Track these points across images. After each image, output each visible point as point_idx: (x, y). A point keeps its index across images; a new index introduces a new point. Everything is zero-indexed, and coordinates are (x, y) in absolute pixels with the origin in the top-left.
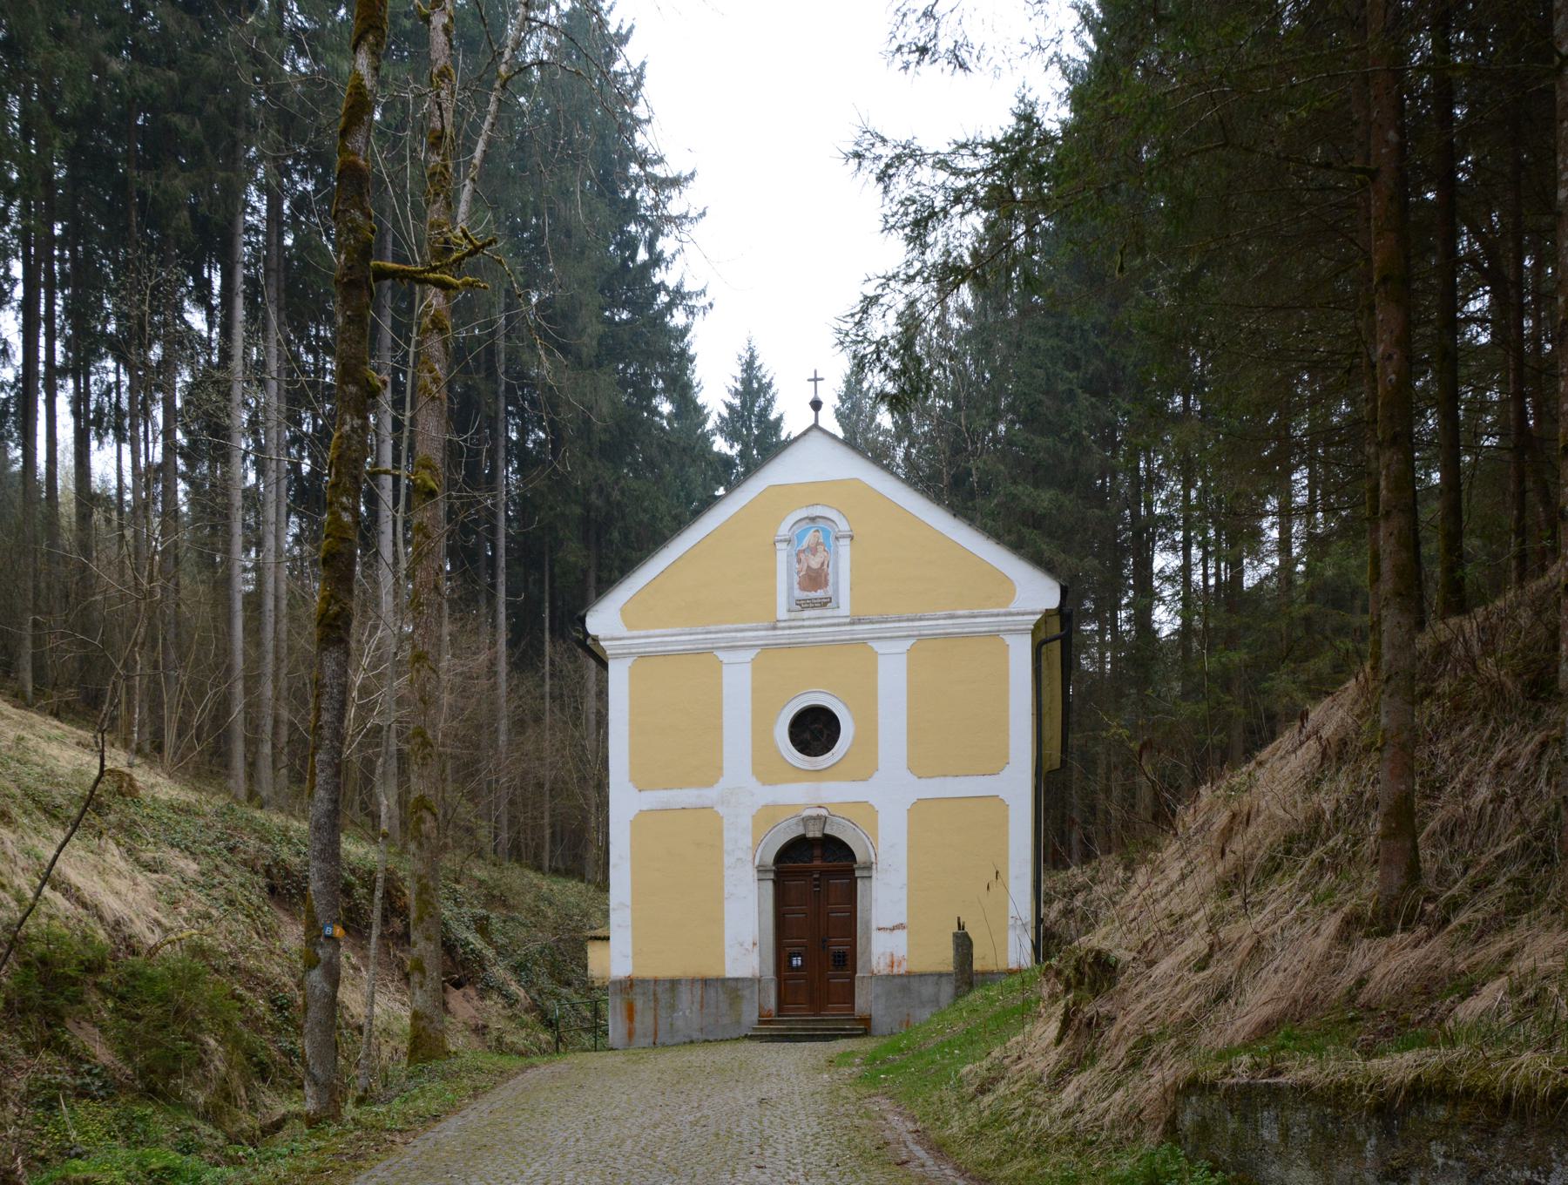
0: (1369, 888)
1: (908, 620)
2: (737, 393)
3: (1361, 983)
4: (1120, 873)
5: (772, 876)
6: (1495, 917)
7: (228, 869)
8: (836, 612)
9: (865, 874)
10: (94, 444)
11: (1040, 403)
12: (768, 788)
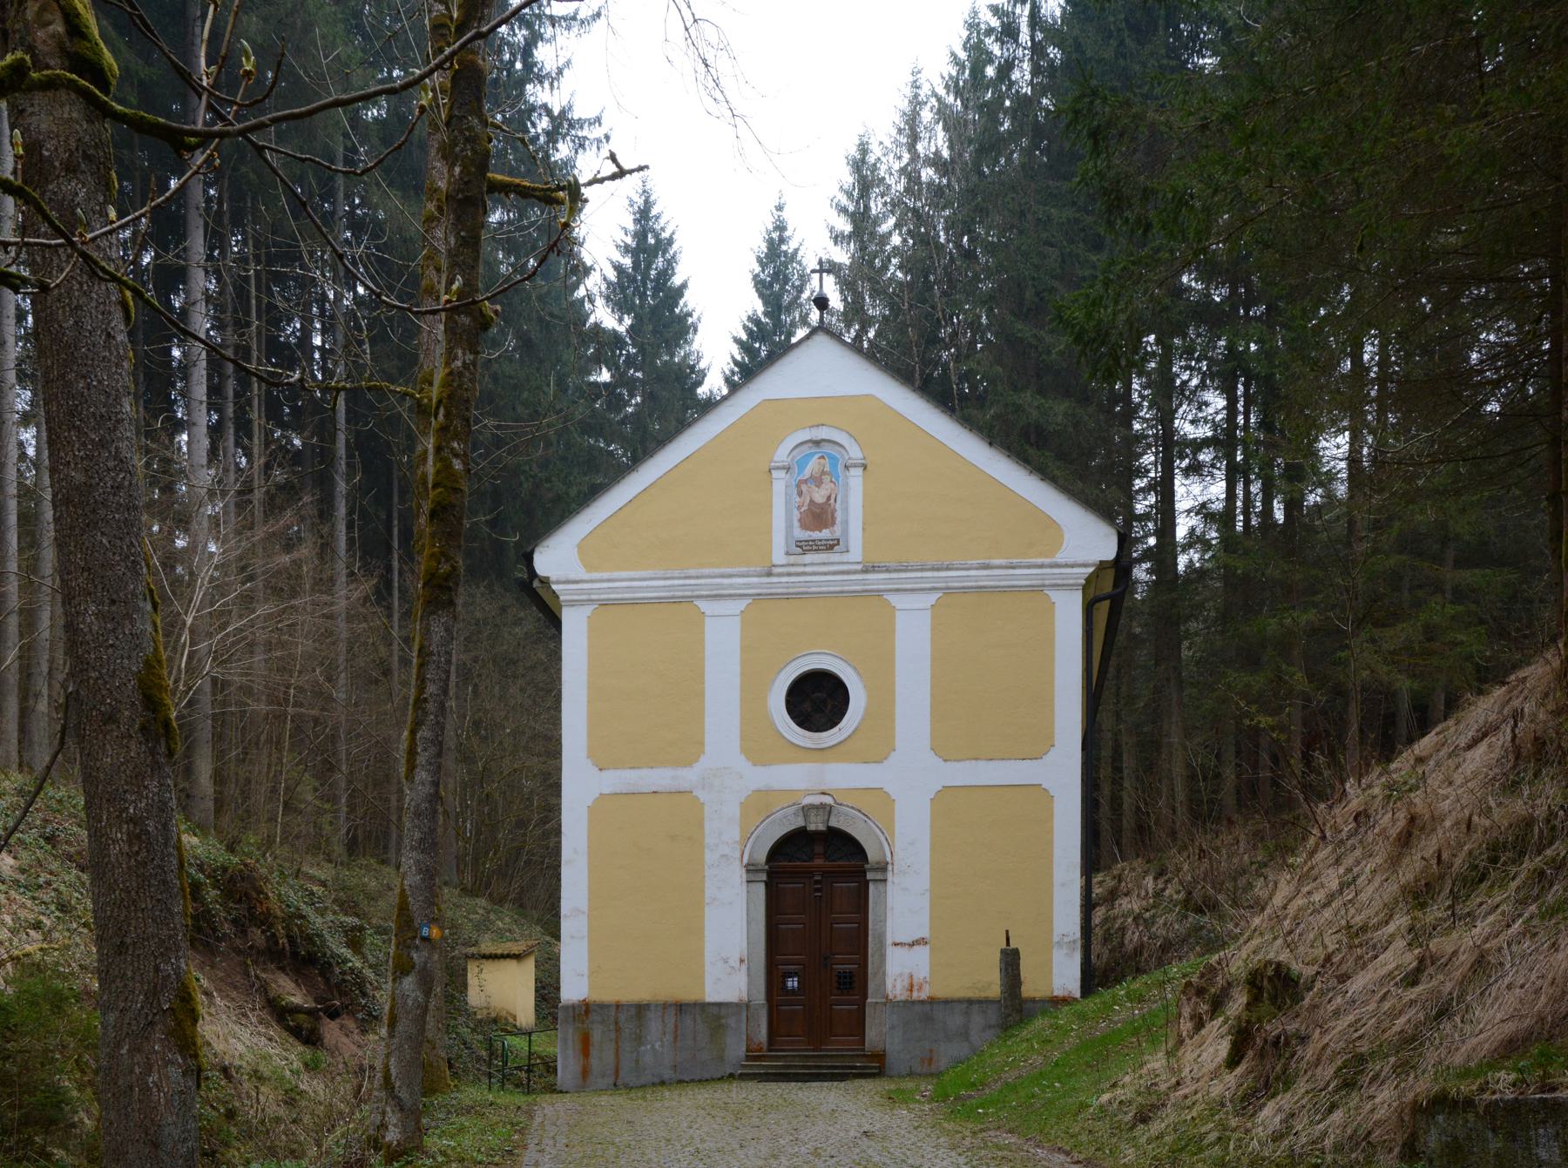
1: (933, 569)
4: (1149, 882)
7: (55, 866)
8: (845, 557)
11: (1052, 290)
12: (760, 770)
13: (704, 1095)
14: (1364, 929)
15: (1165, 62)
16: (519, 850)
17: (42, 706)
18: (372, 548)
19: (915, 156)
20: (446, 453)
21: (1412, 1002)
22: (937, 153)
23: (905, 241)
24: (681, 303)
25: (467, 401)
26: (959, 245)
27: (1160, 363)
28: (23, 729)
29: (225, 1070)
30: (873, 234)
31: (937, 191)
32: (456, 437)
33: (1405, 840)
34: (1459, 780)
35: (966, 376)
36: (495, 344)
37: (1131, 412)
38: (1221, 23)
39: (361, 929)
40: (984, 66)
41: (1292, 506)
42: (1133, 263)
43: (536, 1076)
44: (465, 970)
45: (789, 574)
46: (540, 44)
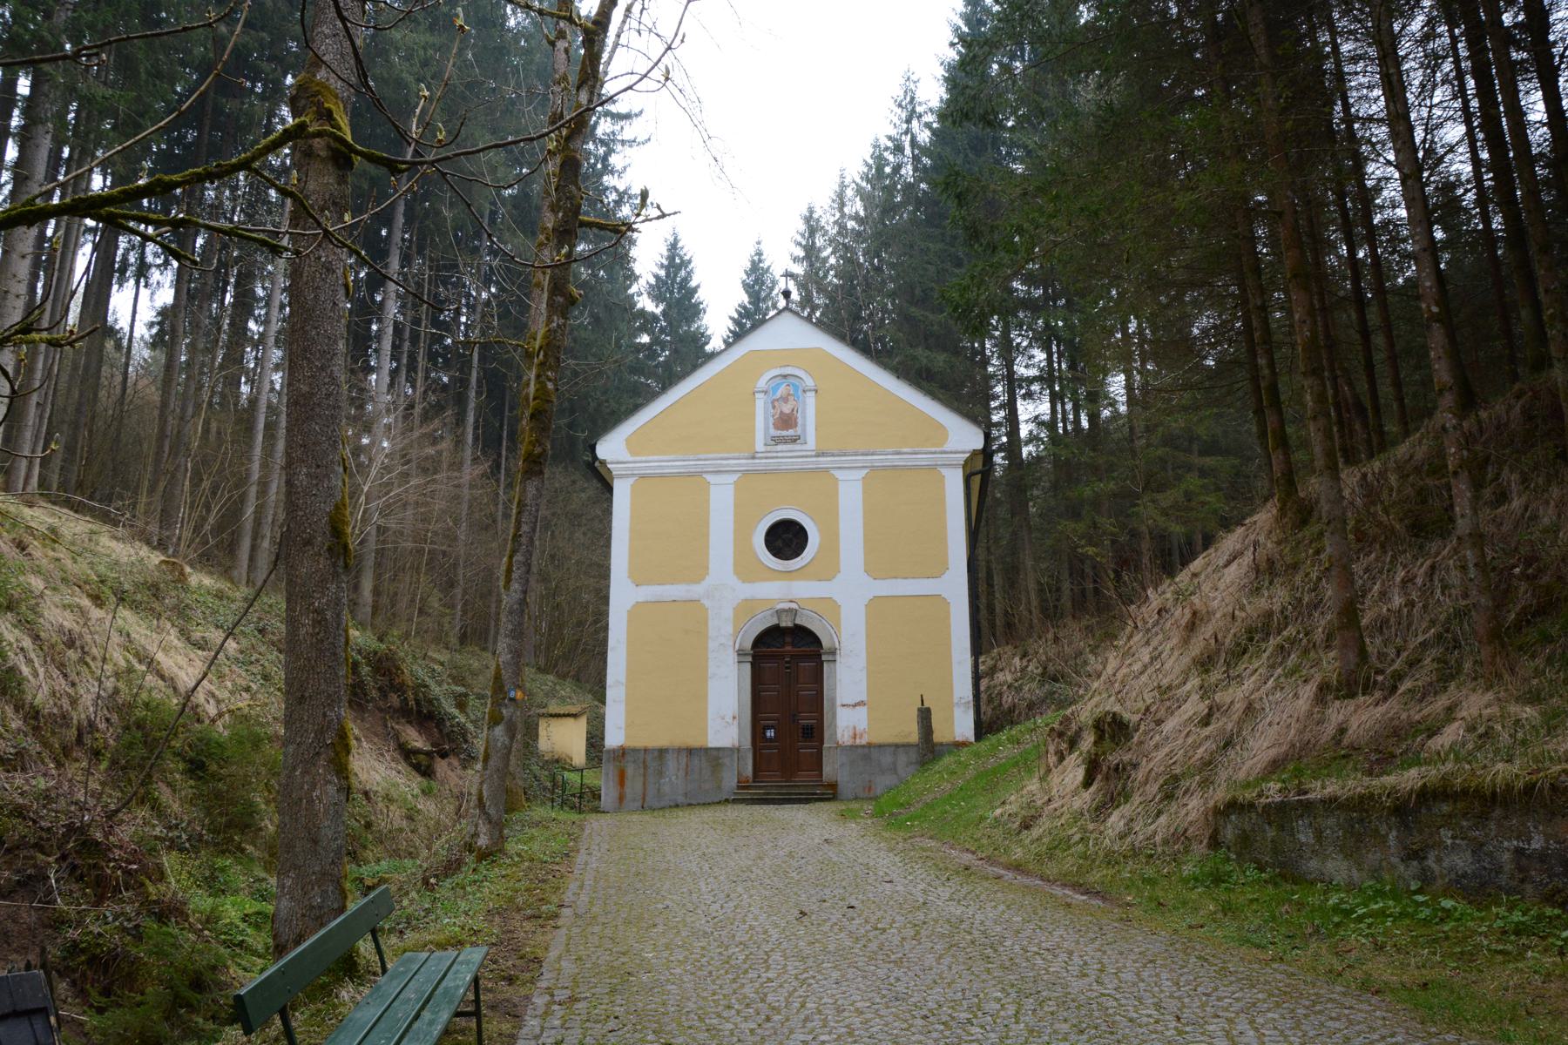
0: (1330, 664)
2: (662, 266)
3: (1342, 730)
4: (1017, 660)
6: (1431, 684)
7: (263, 649)
10: (115, 287)
13: (707, 814)
14: (1170, 688)
16: (579, 641)
17: (266, 544)
18: (489, 442)
19: (843, 215)
20: (543, 378)
21: (1207, 738)
26: (872, 264)
28: (252, 559)
29: (366, 794)
30: (817, 257)
31: (858, 235)
32: (550, 368)
33: (1192, 627)
34: (1222, 586)
35: (880, 339)
37: (986, 361)
38: (1026, 147)
39: (466, 695)
41: (1093, 418)
43: (587, 801)
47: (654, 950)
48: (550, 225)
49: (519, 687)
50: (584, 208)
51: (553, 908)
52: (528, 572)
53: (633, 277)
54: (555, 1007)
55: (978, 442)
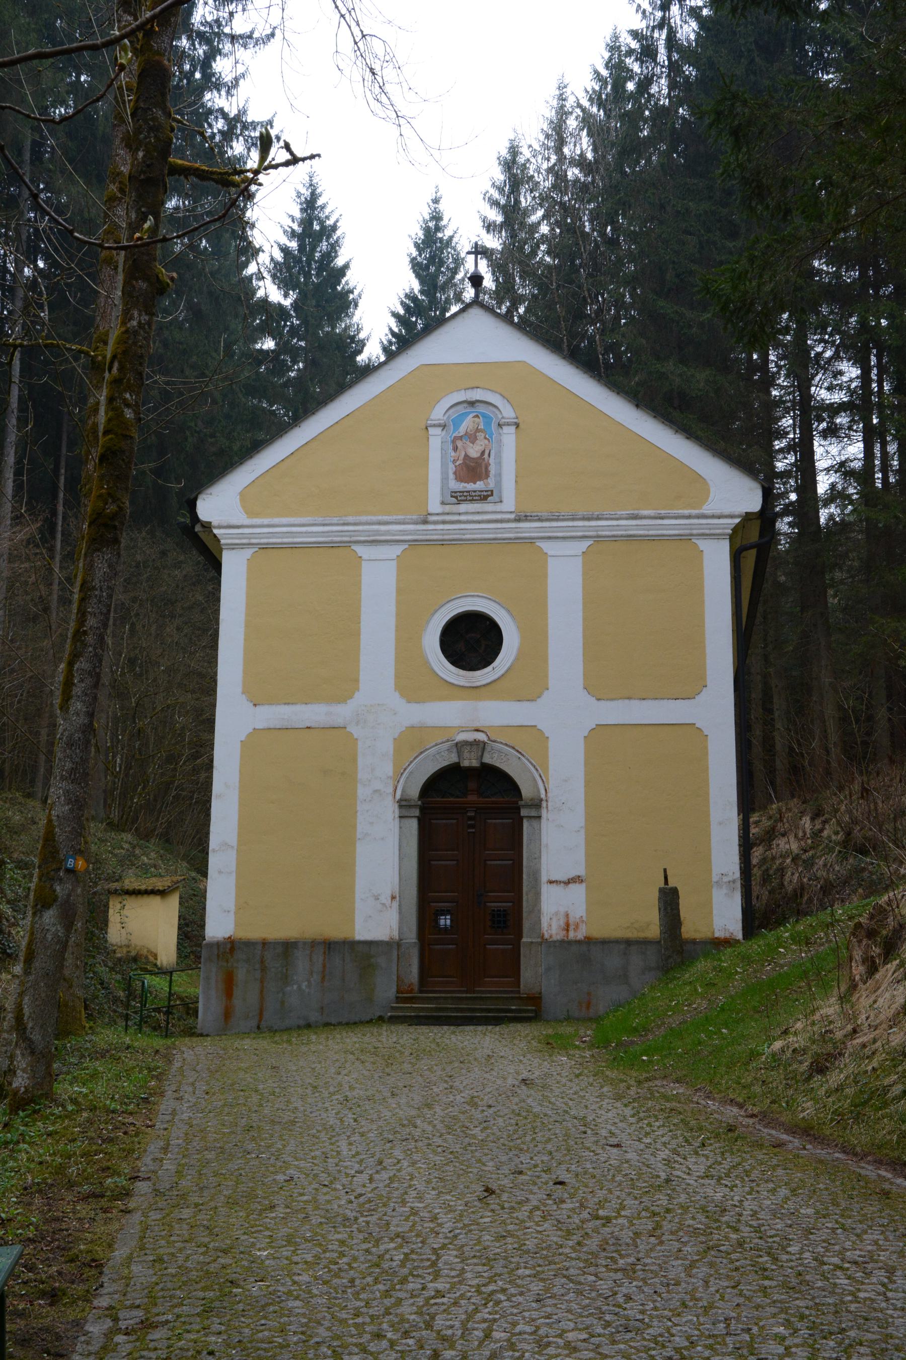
4: (806, 822)
5: (417, 813)
8: (498, 507)
9: (533, 813)
12: (414, 707)
13: (352, 1039)
15: (793, 77)
20: (118, 403)
22: (582, 155)
23: (552, 229)
24: (343, 281)
25: (141, 357)
26: (603, 234)
27: (795, 337)
30: (522, 224)
31: (582, 189)
32: (129, 389)
35: (611, 348)
36: (167, 312)
37: (769, 381)
38: (845, 44)
40: (625, 82)
42: (776, 241)
43: (176, 1018)
44: (107, 906)
45: (444, 522)
46: (218, 58)
47: (270, 1245)
48: (125, 169)
49: (80, 852)
50: (177, 142)
51: (122, 1181)
52: (96, 685)
53: (252, 252)
54: (120, 1338)
55: (753, 501)
